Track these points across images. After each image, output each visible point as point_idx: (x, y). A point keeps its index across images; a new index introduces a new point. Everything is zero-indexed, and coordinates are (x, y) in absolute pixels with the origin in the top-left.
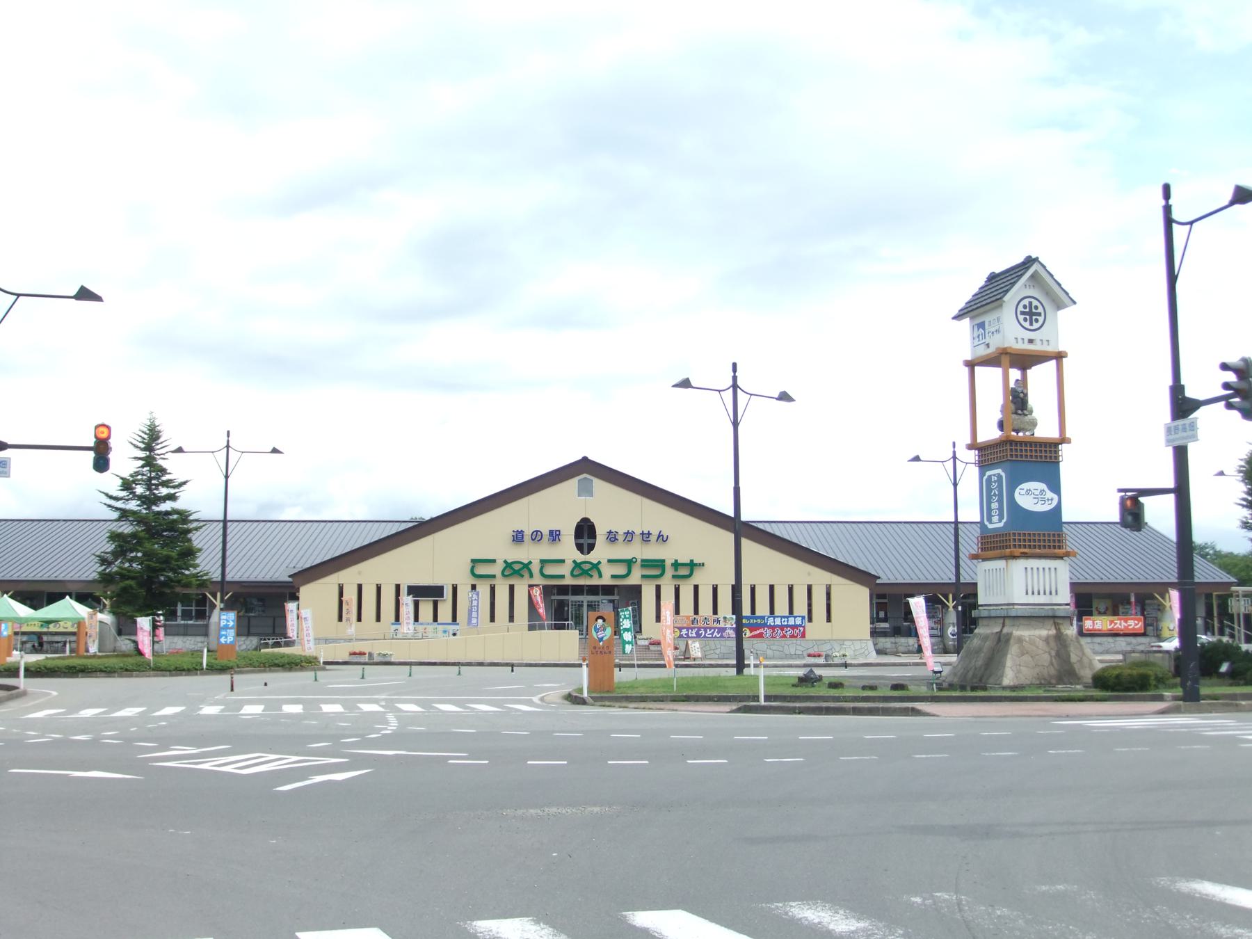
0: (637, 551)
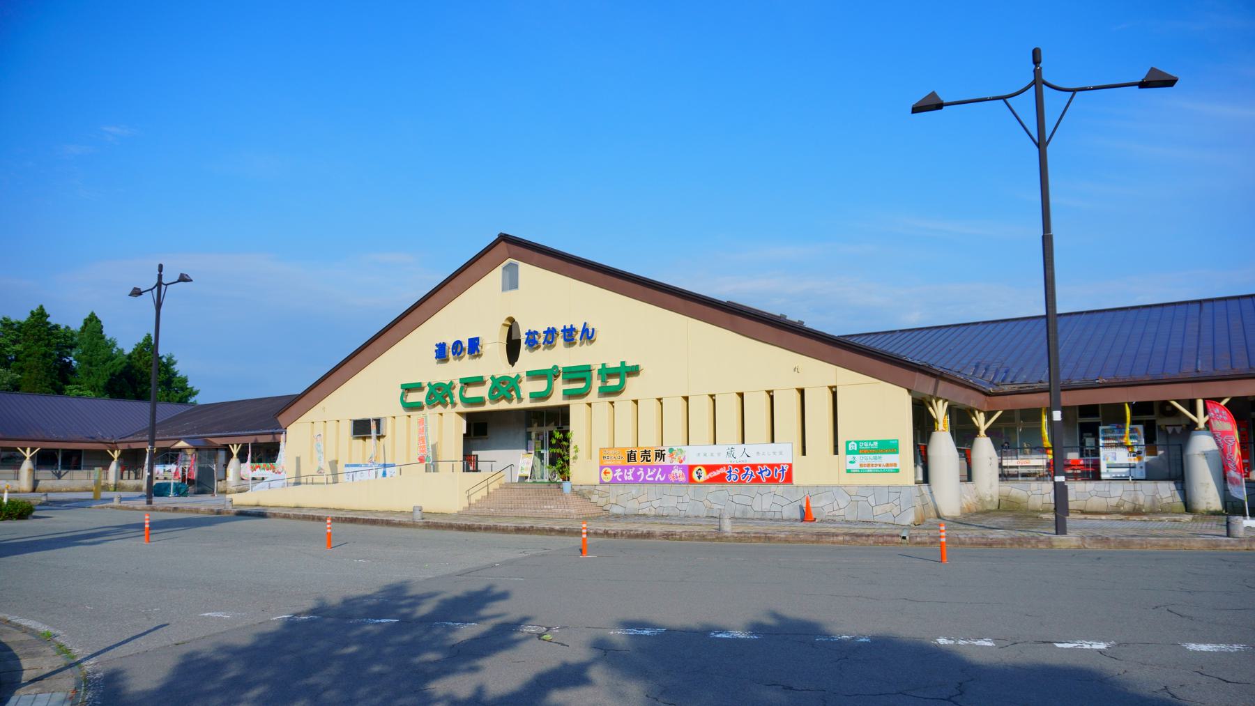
0: (563, 356)
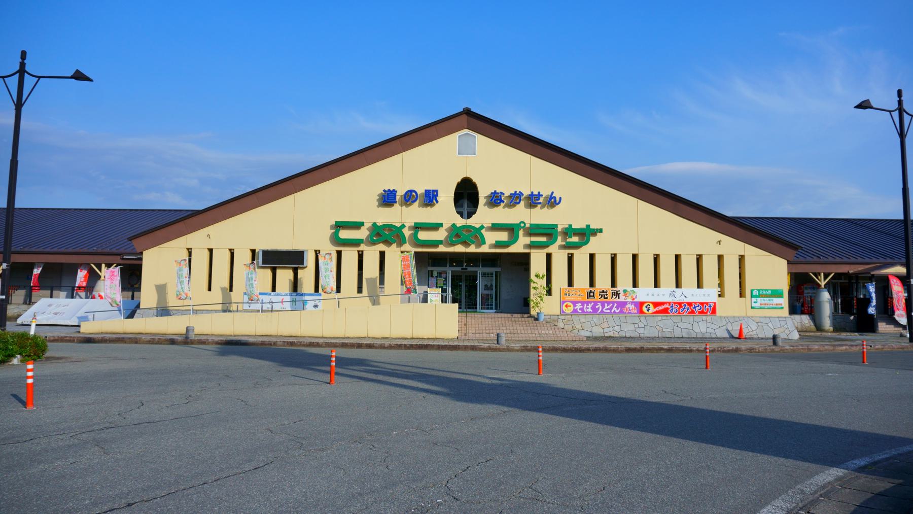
0: (520, 215)
